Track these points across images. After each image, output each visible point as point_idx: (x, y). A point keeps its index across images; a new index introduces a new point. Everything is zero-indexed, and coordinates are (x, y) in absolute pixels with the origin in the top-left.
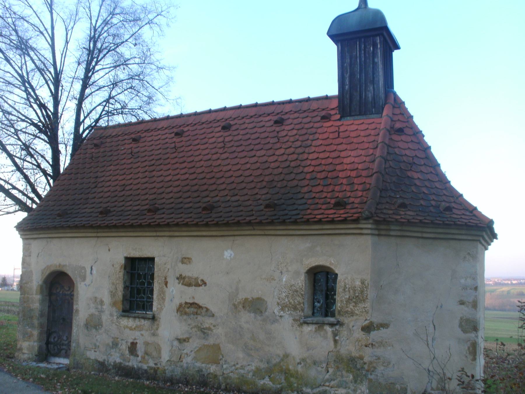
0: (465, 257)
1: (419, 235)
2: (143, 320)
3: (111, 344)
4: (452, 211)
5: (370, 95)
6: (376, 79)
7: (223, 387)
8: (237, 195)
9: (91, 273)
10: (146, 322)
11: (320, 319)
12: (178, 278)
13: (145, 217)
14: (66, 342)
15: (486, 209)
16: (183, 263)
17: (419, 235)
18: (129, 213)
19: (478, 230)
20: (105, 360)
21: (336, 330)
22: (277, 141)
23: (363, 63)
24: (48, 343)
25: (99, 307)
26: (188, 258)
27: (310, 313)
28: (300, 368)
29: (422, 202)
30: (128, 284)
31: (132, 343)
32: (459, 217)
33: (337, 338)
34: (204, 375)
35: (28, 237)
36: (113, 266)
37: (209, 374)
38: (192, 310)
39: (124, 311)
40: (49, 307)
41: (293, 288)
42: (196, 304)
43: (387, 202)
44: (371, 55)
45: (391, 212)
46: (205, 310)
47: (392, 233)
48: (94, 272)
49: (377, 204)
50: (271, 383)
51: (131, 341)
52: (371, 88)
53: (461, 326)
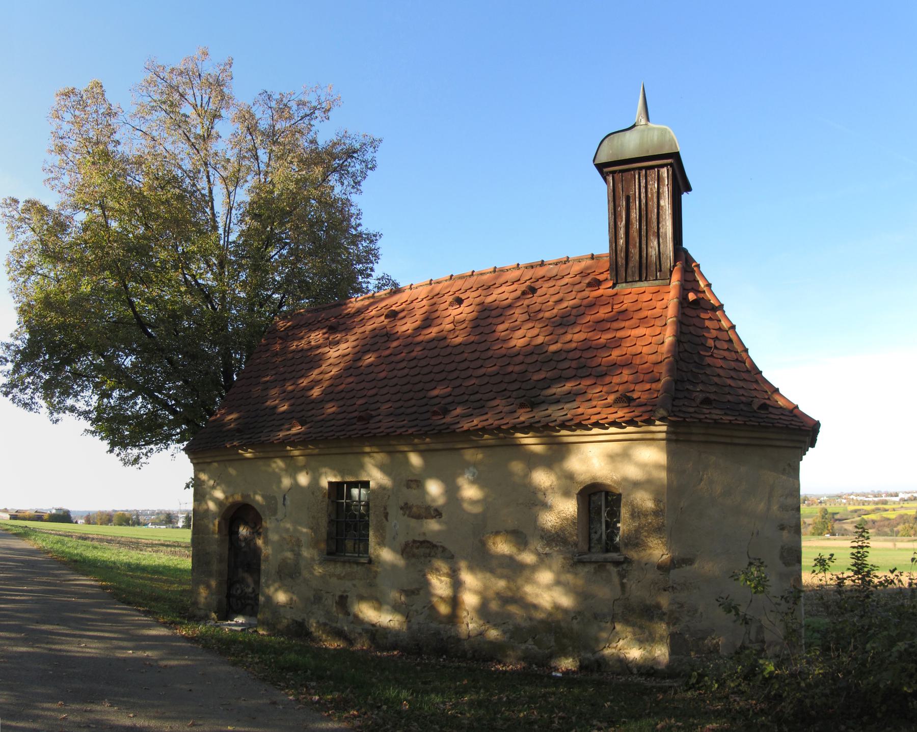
0: (784, 470)
1: (728, 440)
2: (355, 566)
3: (312, 598)
4: (767, 409)
5: (653, 252)
6: (661, 230)
7: (469, 655)
8: (477, 392)
9: (284, 504)
10: (359, 568)
11: (601, 556)
12: (402, 508)
13: (354, 427)
14: (253, 595)
15: (809, 408)
16: (408, 487)
17: (728, 440)
18: (332, 423)
19: (801, 432)
20: (304, 620)
21: (623, 570)
22: (528, 317)
23: (643, 206)
24: (229, 596)
25: (296, 548)
26: (416, 481)
27: (586, 548)
28: (575, 625)
29: (729, 397)
30: (333, 517)
31: (341, 597)
32: (777, 417)
33: (625, 581)
34: (442, 639)
35: (200, 461)
36: (313, 493)
37: (449, 637)
38: (422, 551)
39: (329, 553)
40: (230, 549)
41: (100, 254)
42: (428, 542)
43: (685, 397)
44: (655, 195)
45: (692, 410)
46: (440, 549)
47: (694, 438)
48: (288, 502)
49: (674, 400)
50: (536, 648)
51: (339, 593)
52: (656, 243)
53: (782, 557)
